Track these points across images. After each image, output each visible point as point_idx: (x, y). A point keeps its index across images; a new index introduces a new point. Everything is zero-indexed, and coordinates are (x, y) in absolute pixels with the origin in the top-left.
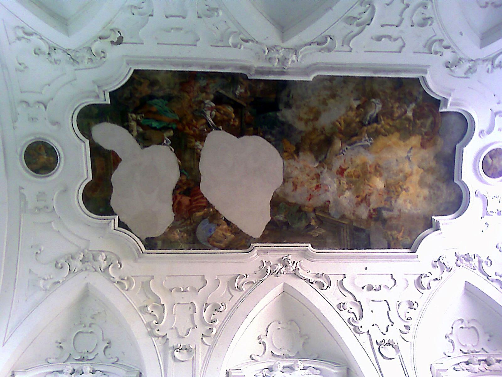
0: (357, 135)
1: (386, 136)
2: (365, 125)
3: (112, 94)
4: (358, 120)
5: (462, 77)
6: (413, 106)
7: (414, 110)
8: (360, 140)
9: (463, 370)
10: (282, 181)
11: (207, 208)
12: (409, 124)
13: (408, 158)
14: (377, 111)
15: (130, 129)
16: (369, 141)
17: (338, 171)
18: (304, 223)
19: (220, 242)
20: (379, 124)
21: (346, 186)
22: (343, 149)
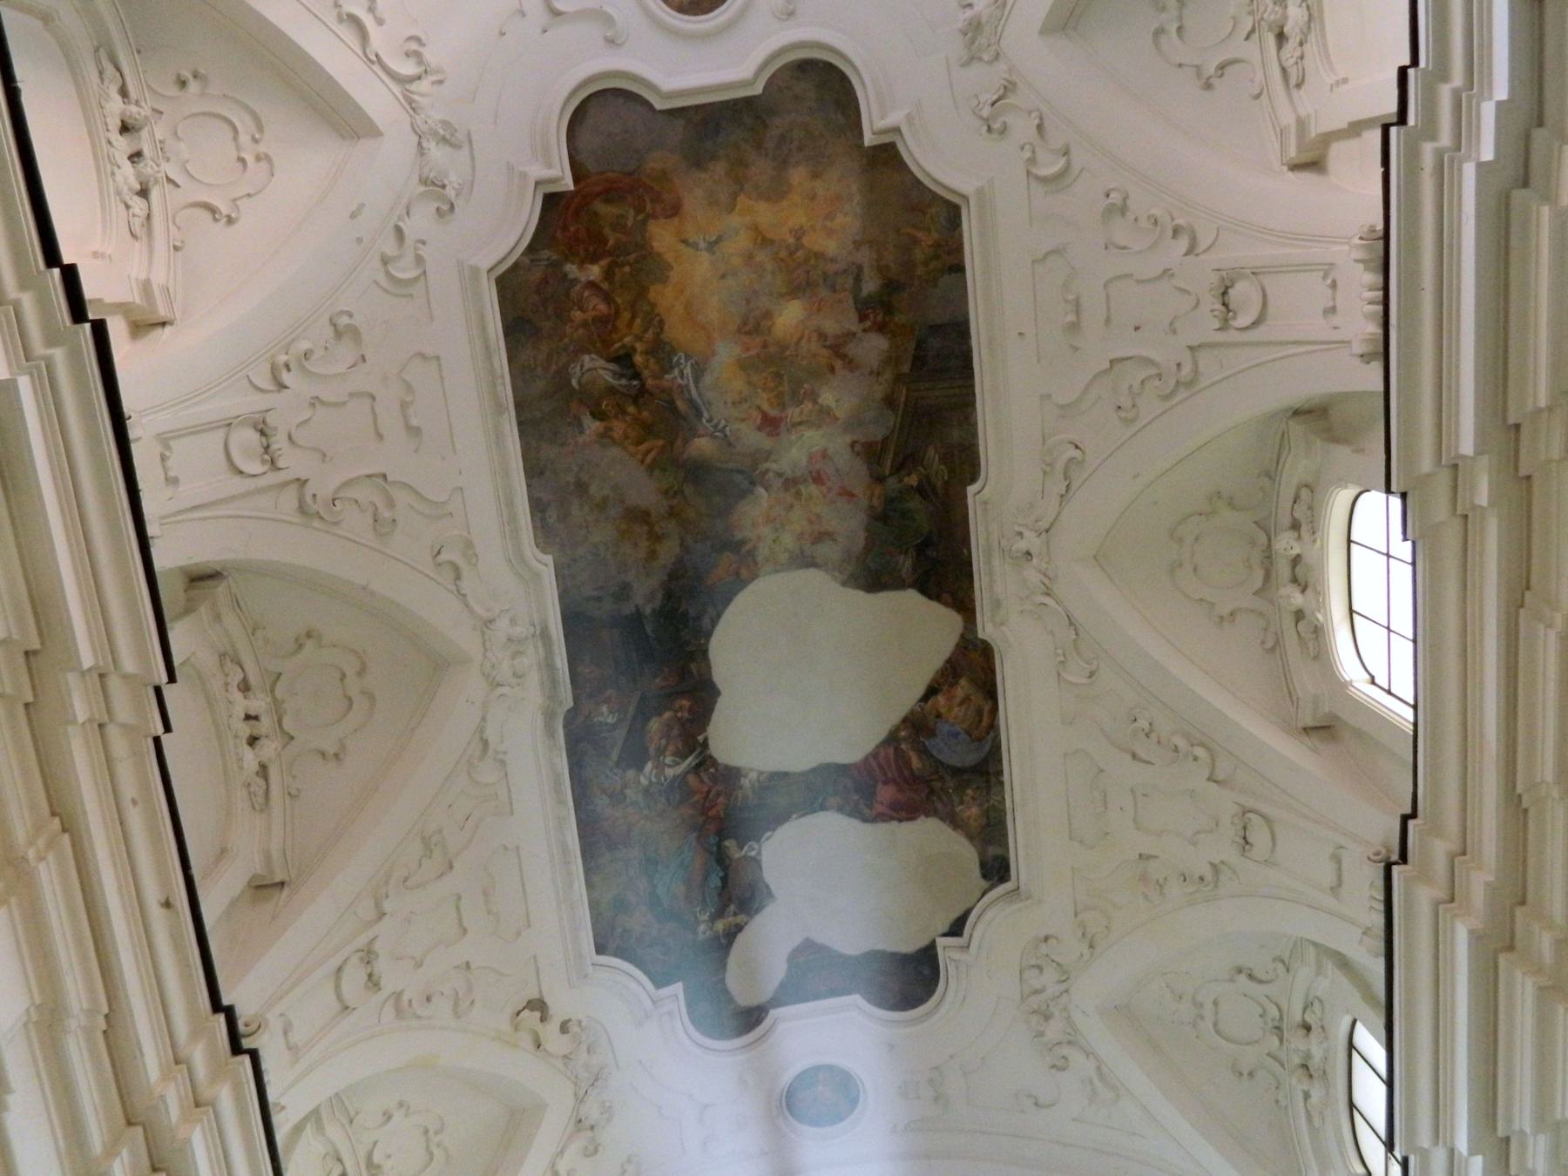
0: (671, 402)
1: (661, 322)
2: (643, 385)
3: (659, 983)
4: (631, 409)
5: (473, 158)
6: (571, 269)
7: (582, 264)
8: (683, 389)
9: (1302, 58)
10: (813, 570)
11: (900, 745)
12: (622, 265)
13: (712, 246)
14: (601, 363)
15: (733, 930)
16: (682, 366)
17: (770, 434)
18: (915, 504)
19: (980, 713)
20: (635, 350)
21: (808, 406)
22: (712, 429)
